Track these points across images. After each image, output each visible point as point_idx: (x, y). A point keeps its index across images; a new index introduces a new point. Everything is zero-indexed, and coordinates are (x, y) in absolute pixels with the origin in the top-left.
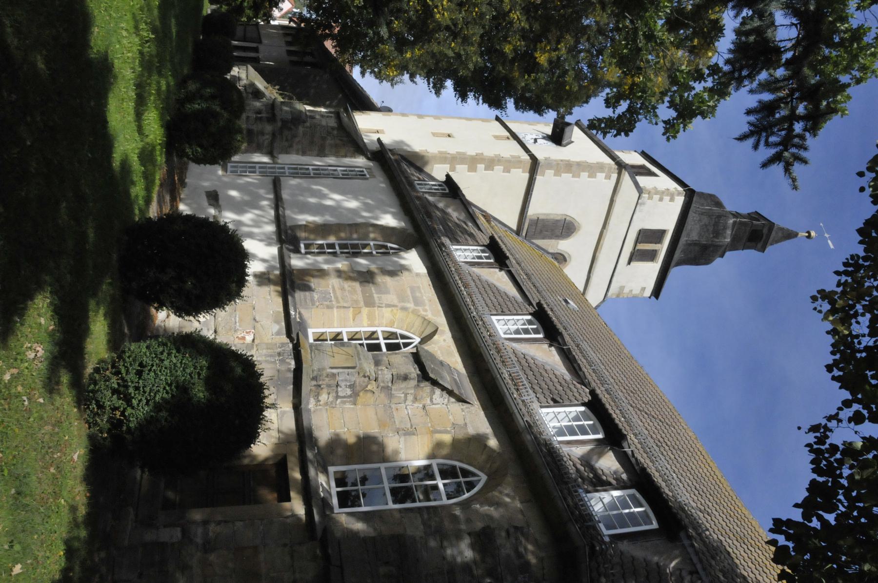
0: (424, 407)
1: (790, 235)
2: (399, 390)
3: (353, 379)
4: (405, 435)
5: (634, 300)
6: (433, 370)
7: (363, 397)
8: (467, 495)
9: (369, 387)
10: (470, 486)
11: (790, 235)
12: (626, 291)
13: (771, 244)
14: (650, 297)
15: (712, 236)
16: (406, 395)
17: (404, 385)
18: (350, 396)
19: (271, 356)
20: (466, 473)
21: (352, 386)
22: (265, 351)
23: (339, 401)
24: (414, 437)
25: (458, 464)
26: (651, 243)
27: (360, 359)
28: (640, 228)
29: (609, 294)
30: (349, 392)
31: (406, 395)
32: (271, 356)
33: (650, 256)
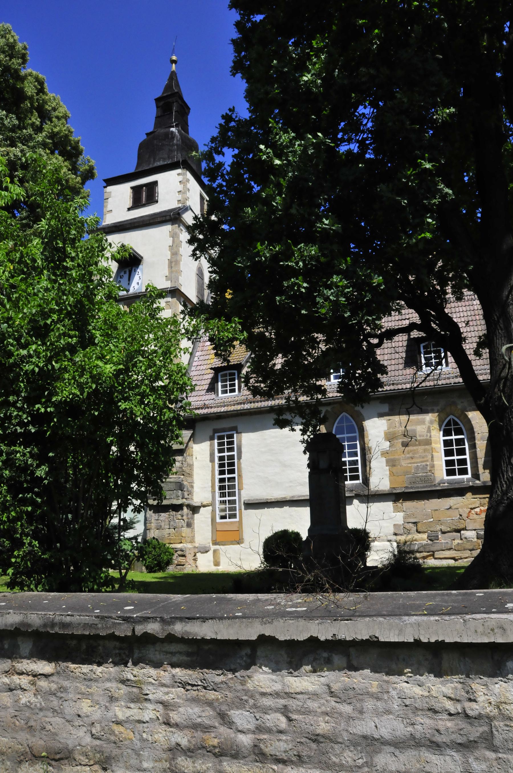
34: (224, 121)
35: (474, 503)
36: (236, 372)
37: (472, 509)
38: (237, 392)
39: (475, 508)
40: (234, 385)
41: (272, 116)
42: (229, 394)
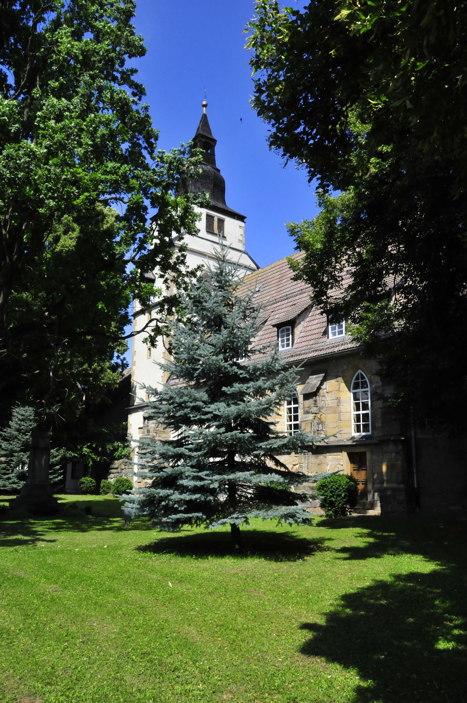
0: (327, 393)
1: (204, 120)
2: (320, 404)
3: (316, 424)
4: (340, 403)
5: (246, 232)
6: (312, 389)
7: (323, 419)
8: (367, 380)
9: (319, 417)
10: (363, 377)
11: (204, 120)
12: (241, 238)
13: (211, 134)
14: (245, 223)
15: (208, 181)
16: (322, 400)
17: (318, 401)
18: (322, 424)
19: (305, 458)
20: (357, 378)
21: (318, 424)
22: (303, 460)
23: (324, 429)
24: (341, 399)
25: (353, 381)
26: (213, 223)
27: (307, 421)
28: (205, 231)
29: (243, 249)
30: (320, 425)
31: (322, 400)
32: (305, 458)
33: (221, 222)
34: (294, 158)
35: (296, 460)
36: (290, 327)
37: (294, 465)
38: (344, 335)
39: (296, 465)
40: (288, 340)
41: (142, 224)
42: (337, 336)
